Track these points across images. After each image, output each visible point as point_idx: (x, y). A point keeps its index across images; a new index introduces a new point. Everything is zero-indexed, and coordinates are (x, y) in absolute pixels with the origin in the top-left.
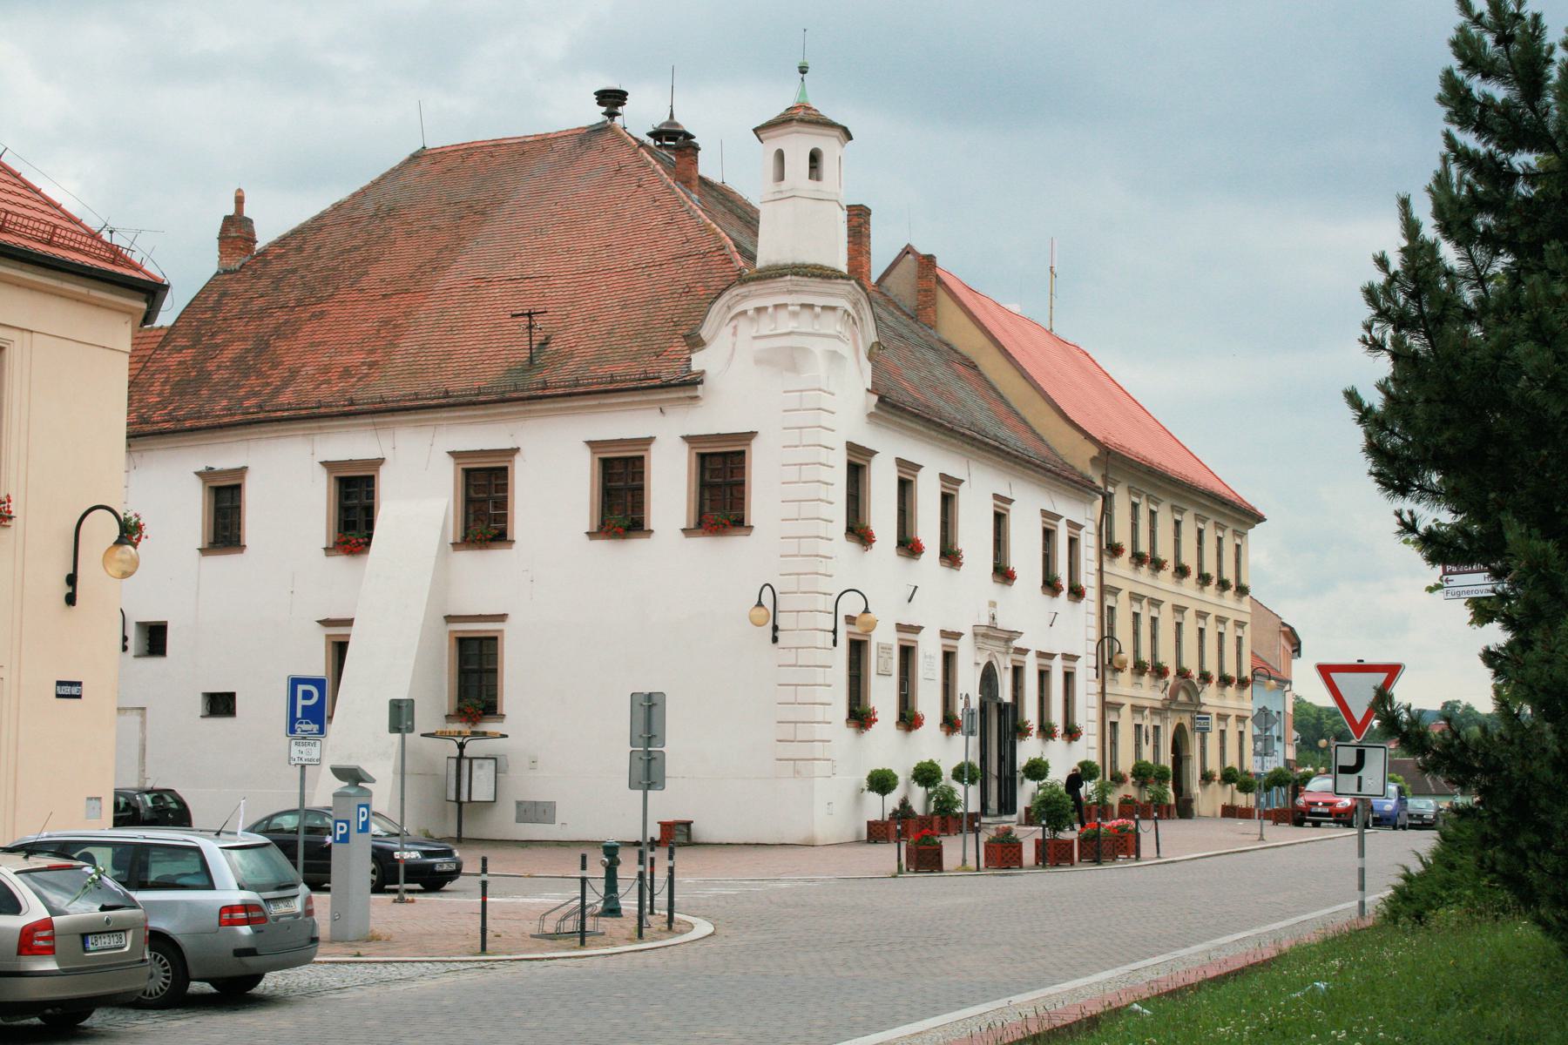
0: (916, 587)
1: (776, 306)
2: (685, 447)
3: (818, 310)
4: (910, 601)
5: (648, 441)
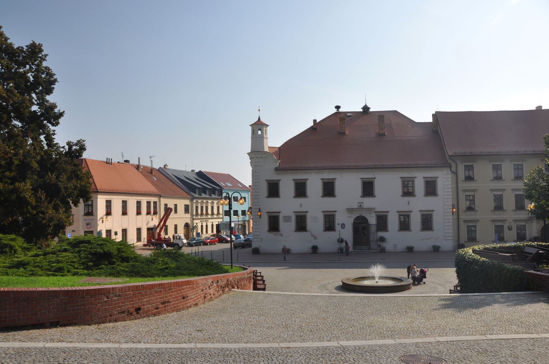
0: (409, 201)
1: (265, 157)
2: (321, 181)
3: (259, 158)
4: (409, 204)
5: (437, 177)
